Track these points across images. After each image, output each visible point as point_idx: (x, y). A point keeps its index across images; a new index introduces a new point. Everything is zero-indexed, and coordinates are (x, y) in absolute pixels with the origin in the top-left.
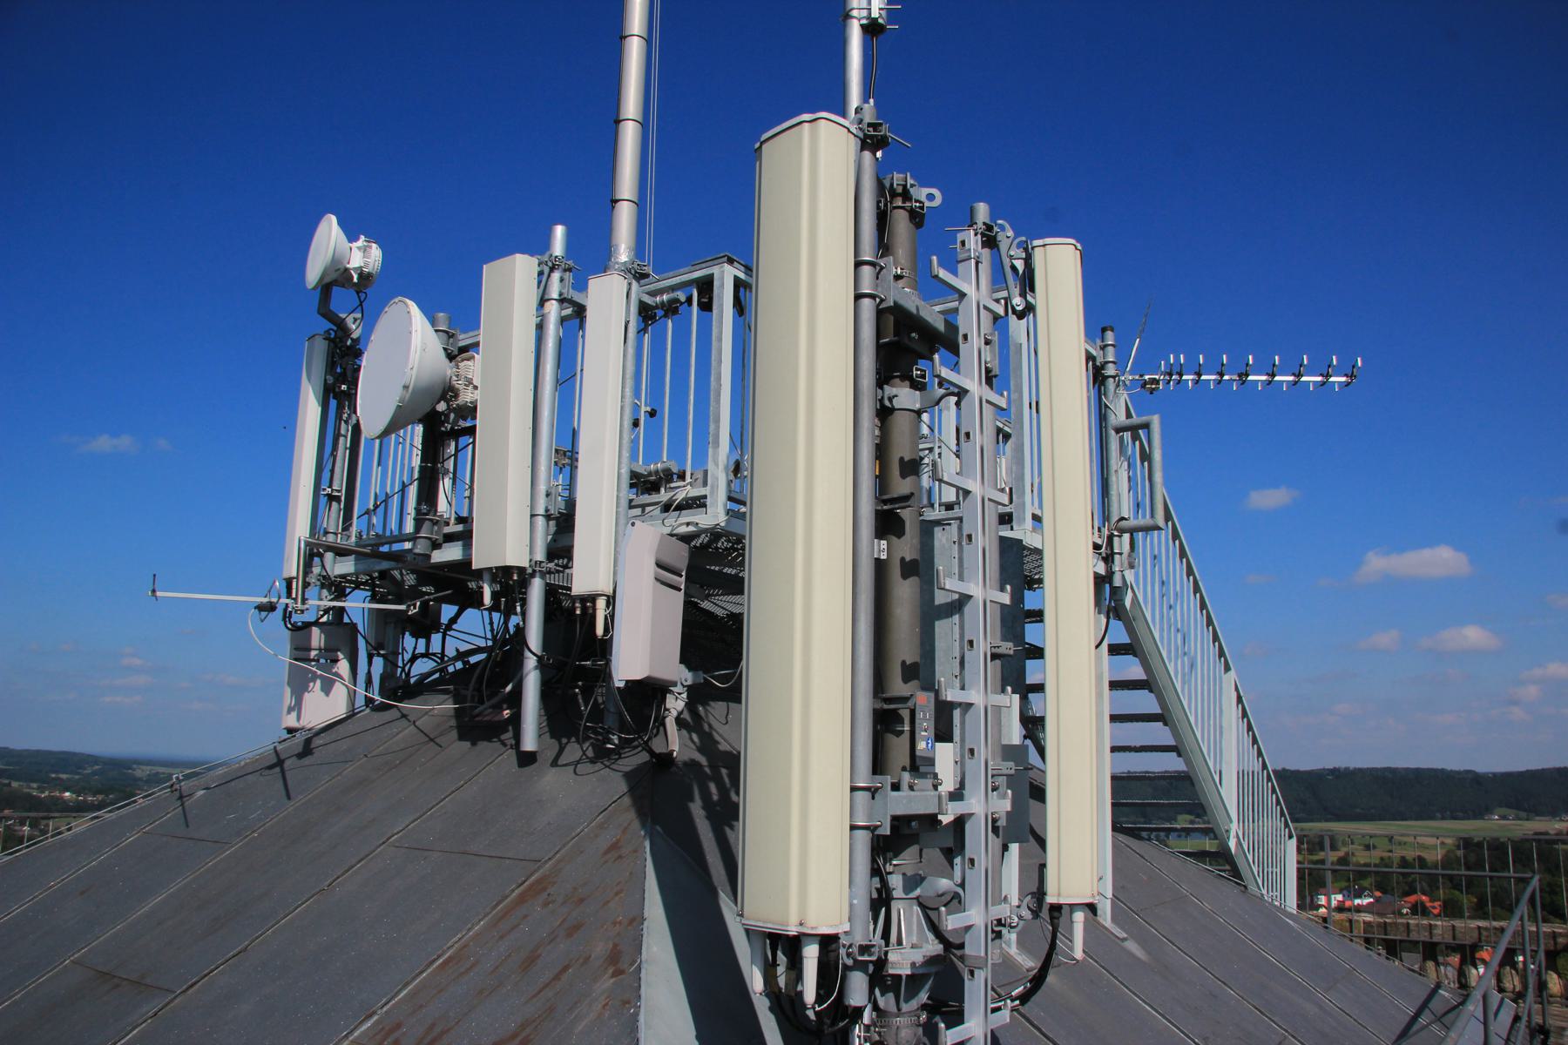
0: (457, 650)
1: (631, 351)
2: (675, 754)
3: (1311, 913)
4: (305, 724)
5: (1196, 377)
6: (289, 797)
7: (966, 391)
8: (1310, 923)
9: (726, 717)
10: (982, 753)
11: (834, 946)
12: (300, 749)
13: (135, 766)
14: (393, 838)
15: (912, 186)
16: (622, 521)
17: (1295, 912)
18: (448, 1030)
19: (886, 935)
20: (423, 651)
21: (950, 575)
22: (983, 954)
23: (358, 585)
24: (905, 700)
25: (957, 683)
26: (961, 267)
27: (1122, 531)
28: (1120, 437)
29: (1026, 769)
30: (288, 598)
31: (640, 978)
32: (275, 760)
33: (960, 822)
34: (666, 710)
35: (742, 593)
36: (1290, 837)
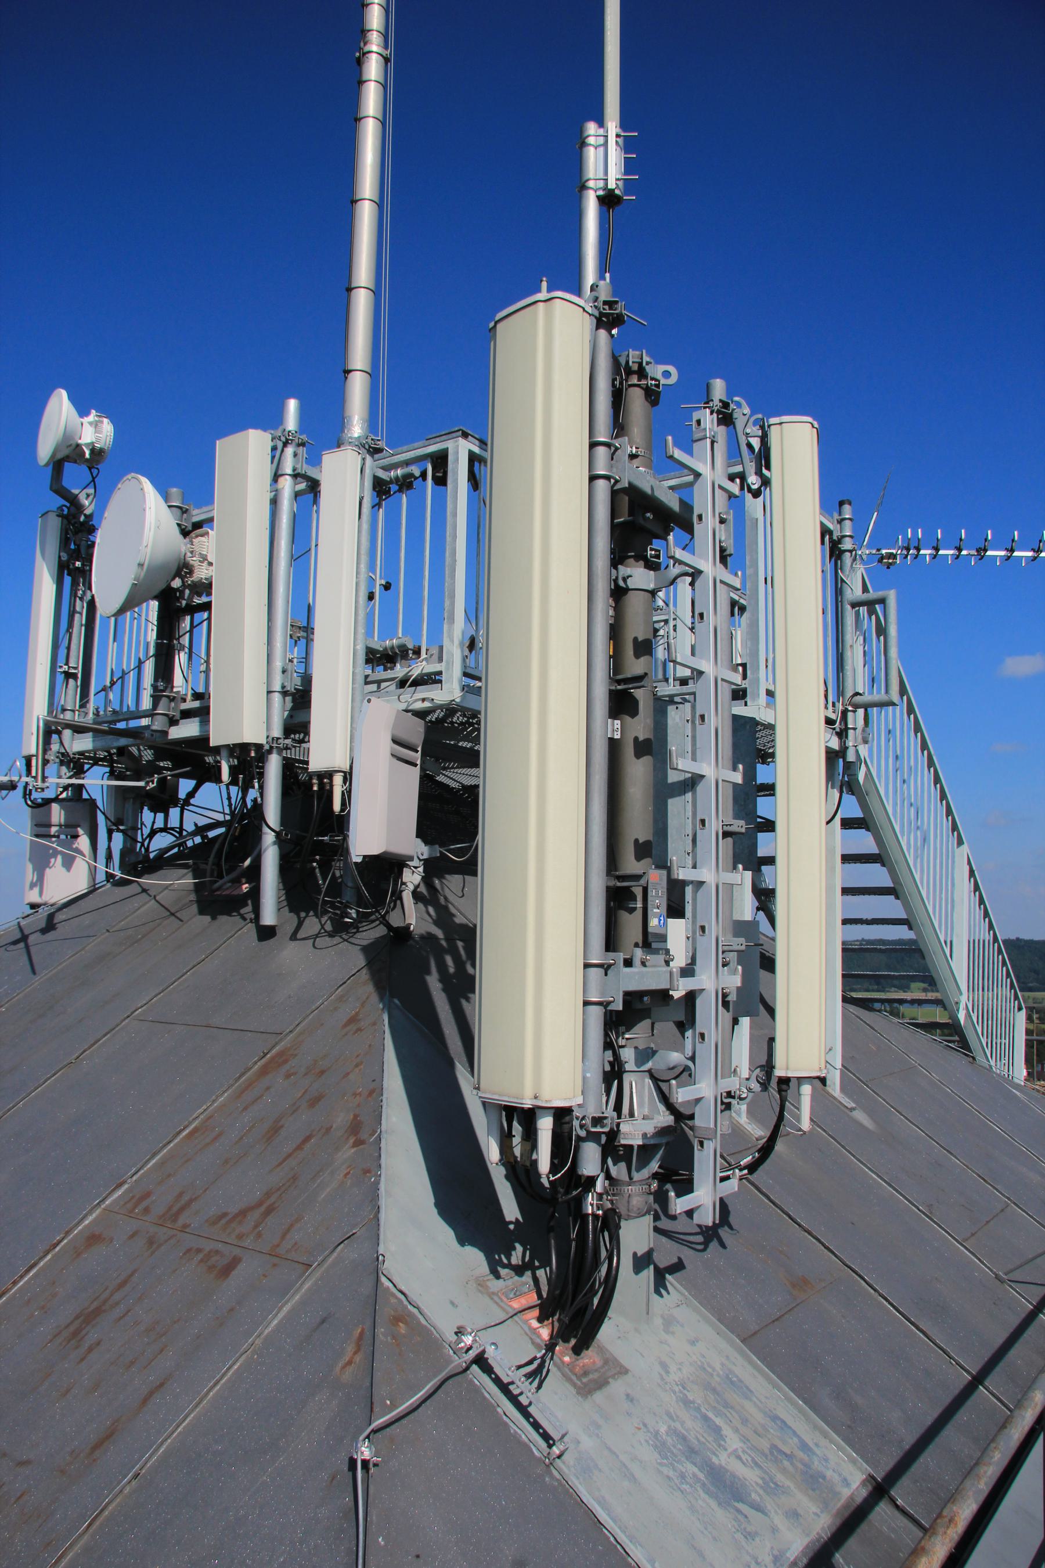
0: (196, 825)
1: (365, 527)
2: (412, 928)
3: (1038, 1083)
4: (47, 899)
5: (934, 552)
6: (34, 972)
7: (700, 572)
8: (1035, 1094)
9: (462, 891)
10: (713, 930)
11: (567, 1119)
12: (43, 925)
14: (137, 1012)
15: (648, 363)
16: (358, 698)
17: (1023, 1084)
18: (196, 1199)
19: (618, 1108)
20: (162, 826)
21: (682, 755)
22: (712, 1126)
23: (96, 762)
24: (637, 877)
25: (689, 861)
26: (696, 446)
27: (856, 707)
28: (855, 612)
29: (756, 945)
30: (28, 776)
31: (380, 1148)
32: (19, 936)
33: (691, 997)
34: (403, 883)
35: (477, 765)
36: (1020, 1009)
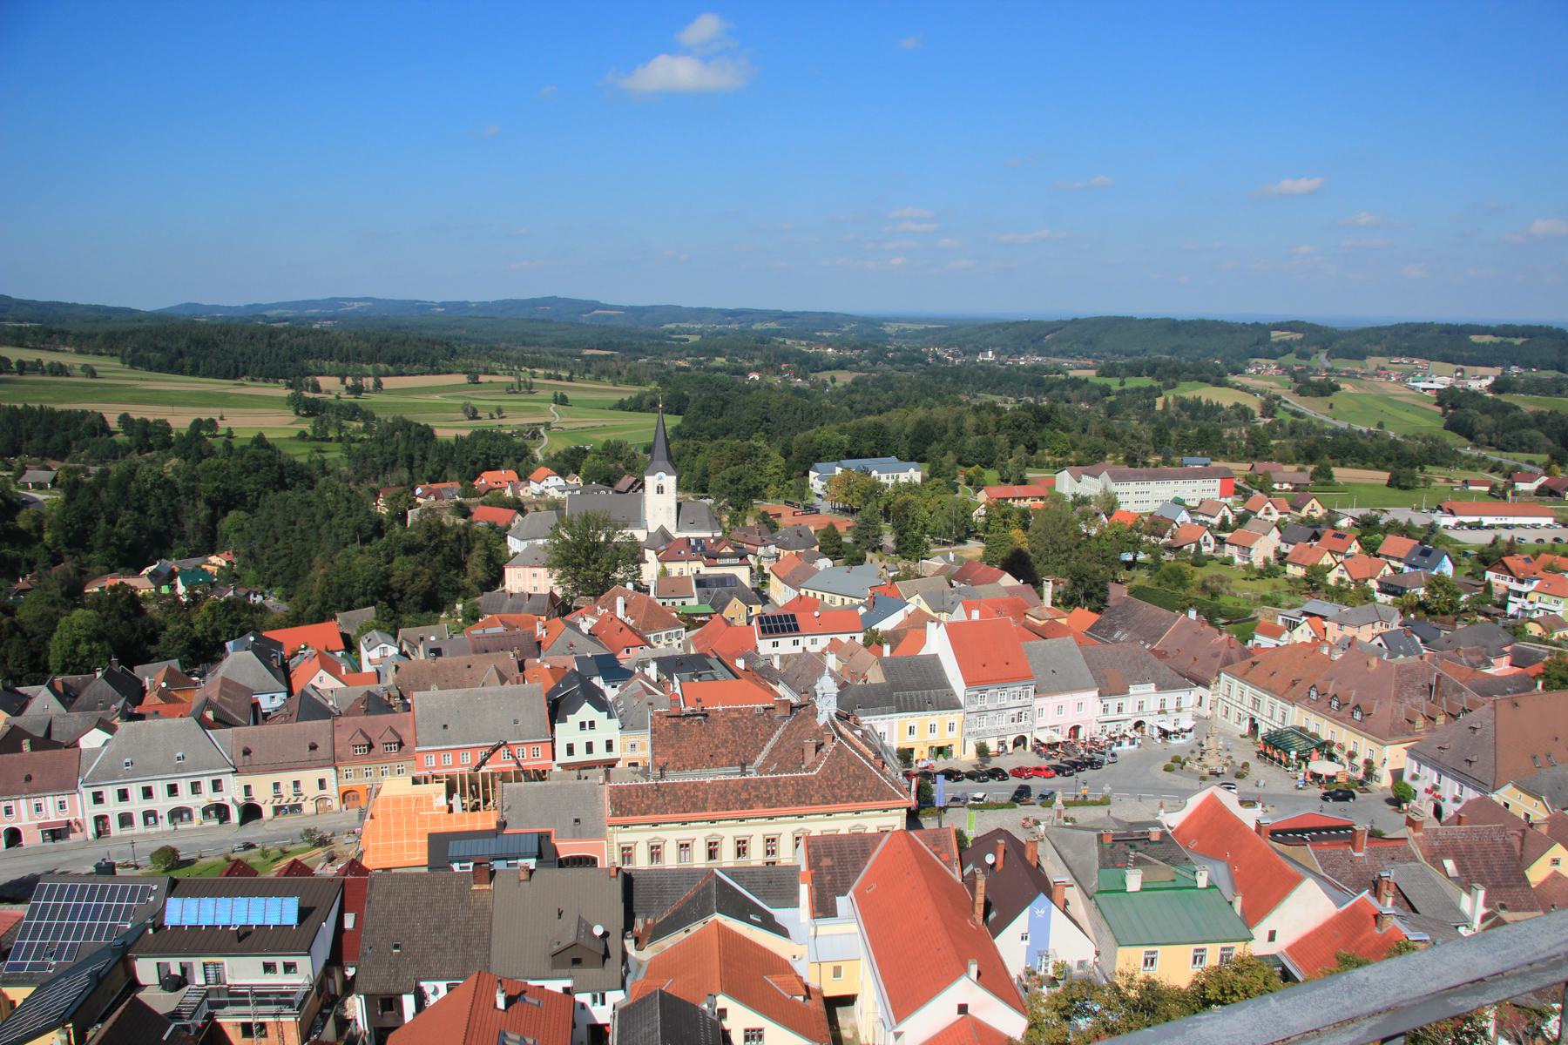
13: (885, 323)
